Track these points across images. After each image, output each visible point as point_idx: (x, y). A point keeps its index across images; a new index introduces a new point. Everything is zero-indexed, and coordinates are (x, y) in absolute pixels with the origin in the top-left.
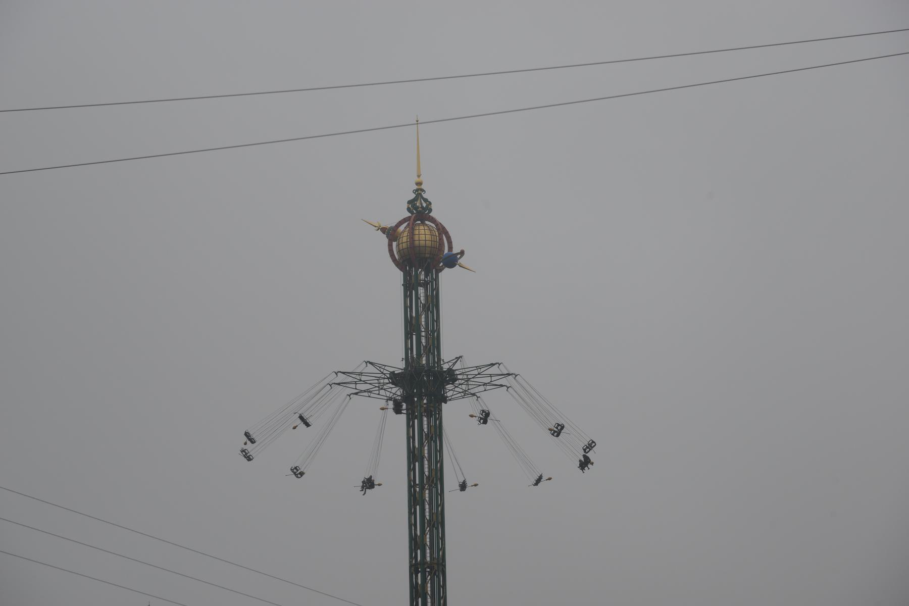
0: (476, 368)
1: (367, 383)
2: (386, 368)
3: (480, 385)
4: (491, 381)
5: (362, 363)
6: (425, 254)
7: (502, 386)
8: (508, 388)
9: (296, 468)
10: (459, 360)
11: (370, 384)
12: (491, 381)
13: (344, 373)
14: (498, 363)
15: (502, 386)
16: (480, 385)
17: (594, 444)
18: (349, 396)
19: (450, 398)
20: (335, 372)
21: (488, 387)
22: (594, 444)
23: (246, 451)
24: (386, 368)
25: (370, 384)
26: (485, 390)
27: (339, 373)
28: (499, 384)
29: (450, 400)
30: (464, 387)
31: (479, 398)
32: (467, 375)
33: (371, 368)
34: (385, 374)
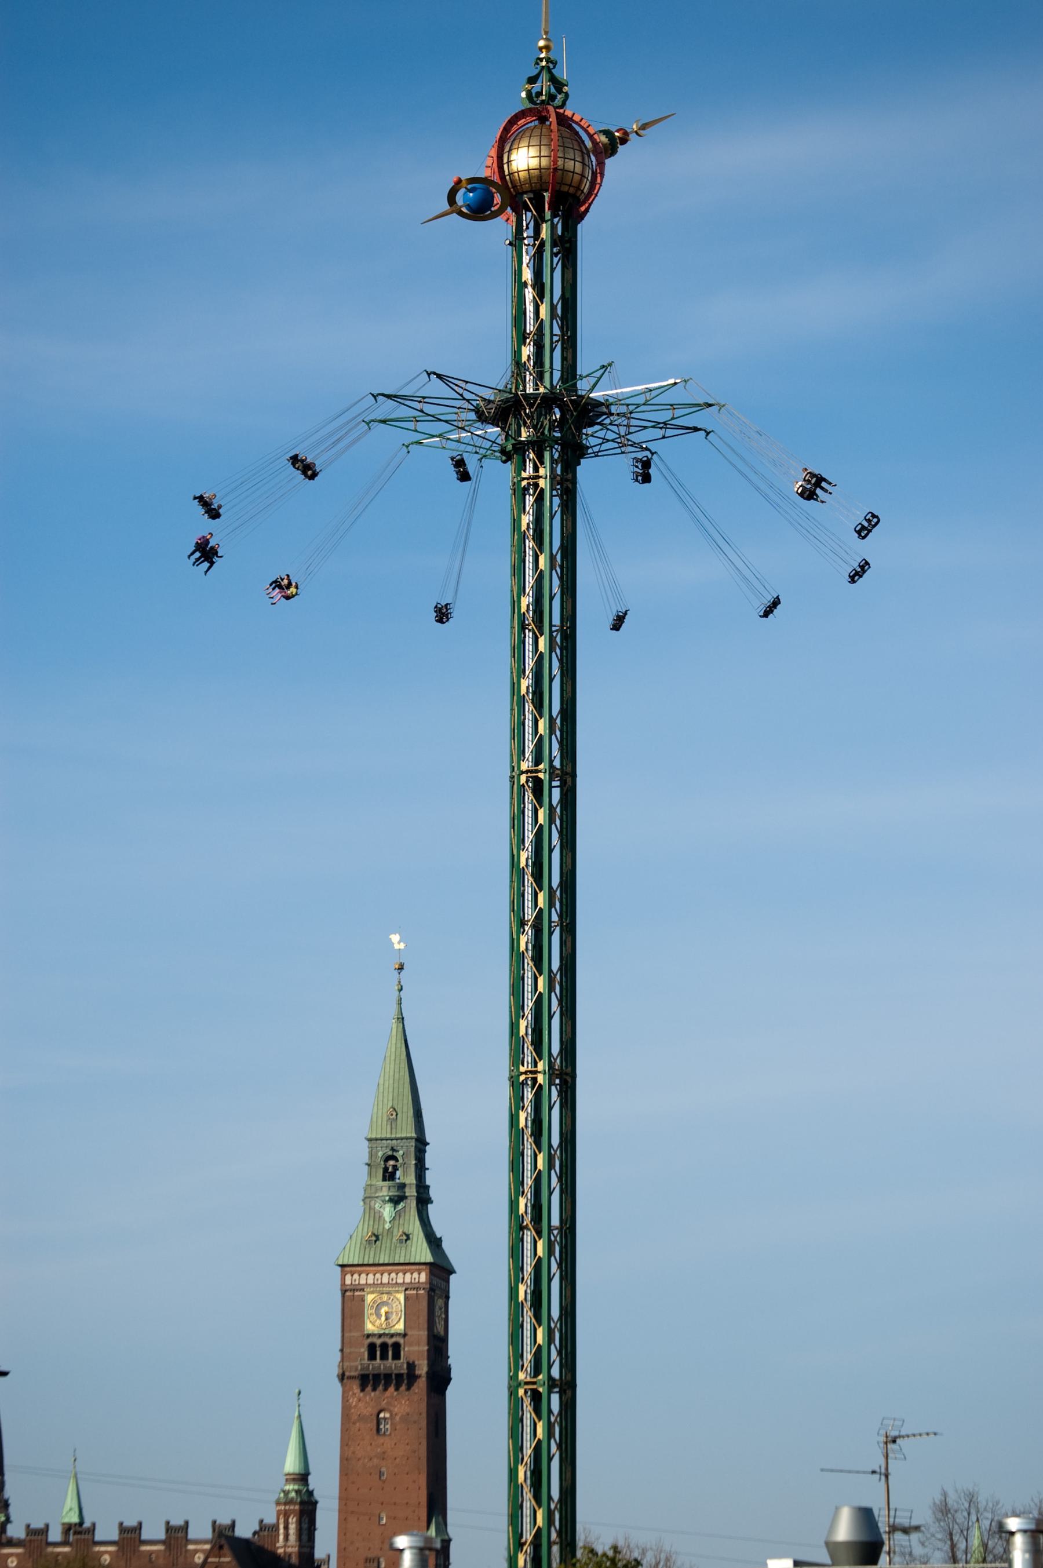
0: (669, 407)
1: (433, 416)
2: (469, 387)
3: (645, 427)
4: (673, 419)
5: (421, 373)
6: (565, 158)
7: (696, 429)
8: (708, 433)
9: (859, 532)
10: (608, 370)
11: (446, 421)
12: (673, 419)
13: (389, 397)
14: (718, 404)
15: (696, 429)
16: (645, 427)
17: (875, 520)
18: (407, 447)
19: (596, 449)
20: (373, 395)
21: (669, 433)
22: (875, 520)
23: (857, 529)
24: (469, 387)
25: (446, 421)
26: (664, 437)
27: (381, 397)
28: (691, 426)
29: (596, 455)
30: (623, 430)
31: (655, 455)
32: (628, 405)
33: (437, 388)
34: (468, 401)
